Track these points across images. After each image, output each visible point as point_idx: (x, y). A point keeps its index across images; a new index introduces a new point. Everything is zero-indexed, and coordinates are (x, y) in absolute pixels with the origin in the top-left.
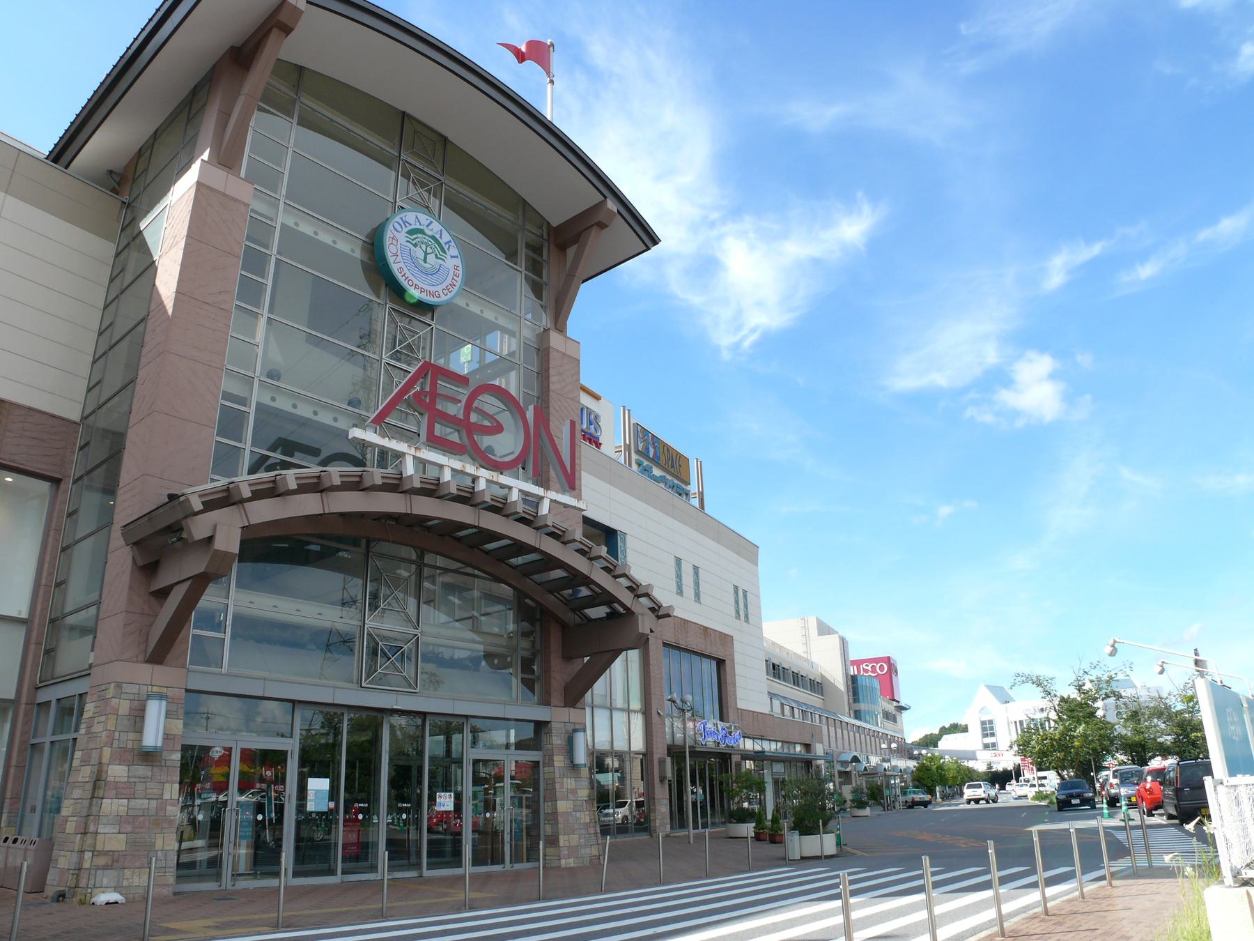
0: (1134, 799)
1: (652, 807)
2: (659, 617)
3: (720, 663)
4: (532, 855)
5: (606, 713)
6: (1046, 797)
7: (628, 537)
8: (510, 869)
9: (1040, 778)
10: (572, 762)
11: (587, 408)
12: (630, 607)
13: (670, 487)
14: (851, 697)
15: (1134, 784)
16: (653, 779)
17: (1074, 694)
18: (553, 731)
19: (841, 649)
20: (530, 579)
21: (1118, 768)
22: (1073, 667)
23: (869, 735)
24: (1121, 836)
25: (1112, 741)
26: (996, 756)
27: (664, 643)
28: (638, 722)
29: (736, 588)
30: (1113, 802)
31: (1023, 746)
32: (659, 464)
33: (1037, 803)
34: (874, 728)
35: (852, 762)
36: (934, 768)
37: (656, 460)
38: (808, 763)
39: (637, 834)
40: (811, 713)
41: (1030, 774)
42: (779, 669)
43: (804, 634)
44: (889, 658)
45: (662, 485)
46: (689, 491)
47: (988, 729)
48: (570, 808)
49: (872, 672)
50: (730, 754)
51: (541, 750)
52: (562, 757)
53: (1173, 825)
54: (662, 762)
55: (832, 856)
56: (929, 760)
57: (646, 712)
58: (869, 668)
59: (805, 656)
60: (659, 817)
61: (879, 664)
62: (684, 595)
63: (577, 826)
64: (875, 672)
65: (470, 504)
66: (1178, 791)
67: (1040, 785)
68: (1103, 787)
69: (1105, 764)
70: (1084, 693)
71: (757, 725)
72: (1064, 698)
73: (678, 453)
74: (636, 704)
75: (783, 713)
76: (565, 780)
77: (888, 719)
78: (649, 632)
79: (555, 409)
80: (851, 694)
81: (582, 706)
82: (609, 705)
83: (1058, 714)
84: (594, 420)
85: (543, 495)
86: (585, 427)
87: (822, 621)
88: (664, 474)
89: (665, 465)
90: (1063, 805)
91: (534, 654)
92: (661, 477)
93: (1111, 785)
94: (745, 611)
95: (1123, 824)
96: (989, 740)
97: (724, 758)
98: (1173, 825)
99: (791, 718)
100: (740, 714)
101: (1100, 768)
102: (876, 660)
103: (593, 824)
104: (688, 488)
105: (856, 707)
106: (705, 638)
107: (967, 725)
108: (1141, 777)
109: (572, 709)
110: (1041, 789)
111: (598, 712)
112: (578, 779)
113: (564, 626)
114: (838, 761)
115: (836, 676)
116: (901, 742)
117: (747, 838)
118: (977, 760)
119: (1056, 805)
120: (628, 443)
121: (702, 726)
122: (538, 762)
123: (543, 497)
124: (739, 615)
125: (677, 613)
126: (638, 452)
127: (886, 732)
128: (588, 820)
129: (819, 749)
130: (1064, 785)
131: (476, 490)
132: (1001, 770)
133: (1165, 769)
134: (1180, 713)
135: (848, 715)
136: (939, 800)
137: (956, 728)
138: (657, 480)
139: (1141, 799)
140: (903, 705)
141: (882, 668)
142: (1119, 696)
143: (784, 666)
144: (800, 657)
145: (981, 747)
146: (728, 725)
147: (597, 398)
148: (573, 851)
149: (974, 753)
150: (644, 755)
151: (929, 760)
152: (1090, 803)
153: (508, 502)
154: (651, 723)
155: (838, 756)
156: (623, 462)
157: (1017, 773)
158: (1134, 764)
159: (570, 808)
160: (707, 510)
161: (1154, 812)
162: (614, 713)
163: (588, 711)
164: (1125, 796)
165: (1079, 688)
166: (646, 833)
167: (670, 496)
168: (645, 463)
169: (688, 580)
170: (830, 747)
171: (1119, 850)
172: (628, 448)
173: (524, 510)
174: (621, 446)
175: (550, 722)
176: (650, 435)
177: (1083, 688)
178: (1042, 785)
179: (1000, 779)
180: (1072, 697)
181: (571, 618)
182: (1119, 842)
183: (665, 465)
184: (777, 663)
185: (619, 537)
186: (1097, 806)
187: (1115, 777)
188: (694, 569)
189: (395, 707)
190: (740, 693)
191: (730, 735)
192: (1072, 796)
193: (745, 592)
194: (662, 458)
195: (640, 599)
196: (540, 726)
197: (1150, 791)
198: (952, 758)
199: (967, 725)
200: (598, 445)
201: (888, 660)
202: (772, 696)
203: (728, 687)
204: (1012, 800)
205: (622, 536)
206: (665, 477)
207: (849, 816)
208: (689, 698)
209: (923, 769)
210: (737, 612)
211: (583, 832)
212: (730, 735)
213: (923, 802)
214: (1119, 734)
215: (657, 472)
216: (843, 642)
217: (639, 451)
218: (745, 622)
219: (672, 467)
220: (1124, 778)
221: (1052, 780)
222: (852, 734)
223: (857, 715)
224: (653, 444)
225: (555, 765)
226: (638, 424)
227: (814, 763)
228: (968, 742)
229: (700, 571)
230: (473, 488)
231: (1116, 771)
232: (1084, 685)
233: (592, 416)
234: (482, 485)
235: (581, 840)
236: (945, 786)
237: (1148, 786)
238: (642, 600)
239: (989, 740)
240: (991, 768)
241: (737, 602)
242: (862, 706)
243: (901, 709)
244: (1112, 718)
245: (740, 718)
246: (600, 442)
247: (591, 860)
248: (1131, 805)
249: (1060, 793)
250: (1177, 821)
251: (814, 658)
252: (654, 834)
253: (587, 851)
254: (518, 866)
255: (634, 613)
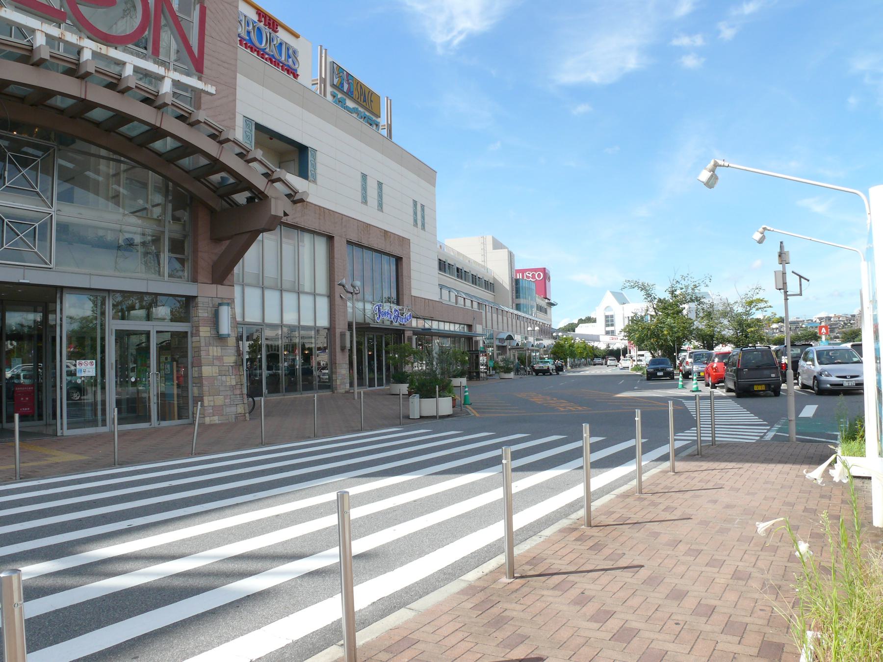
0: (702, 374)
1: (333, 370)
2: (295, 202)
3: (399, 260)
4: (183, 412)
5: (258, 292)
6: (641, 369)
7: (318, 153)
8: (158, 426)
9: (639, 355)
10: (218, 332)
11: (286, 43)
12: (263, 190)
13: (362, 118)
14: (514, 294)
15: (704, 363)
16: (335, 349)
17: (667, 296)
18: (199, 305)
19: (508, 260)
20: (175, 165)
21: (693, 350)
22: (669, 277)
23: (533, 323)
24: (690, 405)
25: (691, 332)
26: (613, 339)
27: (347, 241)
28: (323, 304)
29: (415, 203)
30: (687, 375)
31: (629, 332)
32: (353, 98)
33: (635, 373)
34: (530, 317)
35: (507, 339)
36: (567, 346)
37: (349, 94)
38: (469, 339)
39: (320, 391)
40: (492, 307)
41: (634, 352)
42: (462, 272)
43: (483, 248)
44: (545, 269)
45: (355, 115)
46: (379, 123)
47: (609, 321)
48: (216, 373)
49: (532, 278)
50: (404, 330)
51: (190, 322)
52: (209, 328)
53: (731, 397)
54: (343, 335)
55: (448, 416)
56: (564, 340)
57: (331, 296)
58: (530, 275)
59: (483, 264)
60: (340, 378)
61: (537, 273)
62: (369, 203)
63: (222, 388)
64: (535, 278)
65: (75, 76)
66: (738, 372)
67: (638, 361)
68: (681, 364)
69: (684, 347)
70: (675, 296)
71: (429, 310)
72: (660, 299)
73: (370, 91)
74: (322, 286)
75: (456, 303)
76: (211, 348)
77: (541, 311)
78: (282, 215)
79: (211, 11)
80: (514, 292)
81: (230, 284)
82: (297, 289)
83: (655, 311)
84: (293, 54)
85: (164, 74)
86: (284, 59)
87: (497, 240)
88: (356, 106)
89: (358, 99)
90: (652, 376)
91: (185, 236)
92: (353, 108)
93: (687, 363)
94: (422, 221)
95: (693, 394)
96: (610, 329)
97: (398, 334)
98: (731, 397)
99: (478, 310)
100: (413, 300)
101: (680, 351)
102: (536, 270)
103: (239, 386)
104: (378, 120)
105: (518, 301)
106: (385, 239)
107: (596, 318)
108: (710, 357)
109: (220, 287)
110: (639, 363)
111: (249, 291)
112: (224, 348)
113: (212, 211)
114: (496, 339)
115: (504, 279)
116: (547, 327)
117: (399, 395)
118: (600, 341)
119: (646, 375)
120: (323, 76)
121: (377, 307)
122: (187, 332)
123: (164, 77)
124: (417, 224)
125: (310, 199)
126: (333, 85)
127: (537, 319)
128: (234, 383)
129: (479, 329)
130: (653, 362)
131: (81, 62)
132: (616, 349)
133: (730, 353)
134: (740, 315)
135: (511, 307)
136: (569, 368)
137: (589, 320)
138: (351, 111)
139: (708, 375)
140: (552, 302)
141: (539, 276)
142: (700, 303)
143: (450, 263)
144: (479, 264)
145: (604, 333)
146: (400, 307)
147: (297, 36)
148: (217, 410)
149: (598, 336)
150: (328, 329)
151: (564, 340)
152: (670, 376)
153: (160, 94)
154: (334, 305)
155: (498, 334)
156: (386, 136)
157: (625, 351)
158: (705, 349)
159: (216, 373)
160: (393, 140)
161: (716, 385)
162: (366, 303)
163: (237, 289)
164: (696, 372)
165: (672, 292)
166: (328, 390)
167: (365, 127)
168: (340, 95)
169: (372, 192)
170: (492, 328)
171: (686, 421)
172: (324, 81)
173: (173, 103)
174: (317, 80)
175: (197, 297)
176: (345, 73)
177: (675, 293)
178: (641, 361)
179: (617, 354)
180: (667, 299)
181: (217, 204)
182: (686, 411)
183: (358, 99)
184: (460, 267)
185: (309, 153)
186: (675, 377)
187: (690, 357)
188: (378, 184)
189: (21, 281)
190: (414, 284)
191: (402, 316)
192: (658, 370)
193: (423, 206)
194: (356, 93)
195: (274, 184)
196: (189, 301)
197: (716, 370)
198: (581, 340)
199: (596, 318)
200: (296, 76)
201: (544, 270)
202: (441, 287)
203: (404, 279)
204: (619, 370)
205: (312, 152)
206: (357, 109)
207: (498, 378)
208: (358, 283)
209: (558, 346)
210: (415, 221)
211: (229, 393)
212: (402, 316)
213: (541, 370)
214: (697, 327)
215: (350, 104)
216: (511, 255)
217: (334, 84)
218: (422, 229)
219: (365, 101)
220: (697, 358)
221: (648, 356)
222: (510, 320)
223: (518, 307)
224: (348, 80)
225: (200, 335)
226: (334, 62)
227: (474, 339)
228: (597, 329)
229: (384, 187)
230: (79, 60)
231: (692, 353)
232: (676, 291)
233: (291, 51)
234: (86, 55)
235: (227, 401)
236: (574, 358)
237: (715, 365)
238: (278, 185)
239: (610, 329)
240: (609, 347)
241: (415, 213)
242: (522, 301)
243: (551, 304)
244: (693, 316)
245: (413, 303)
246: (298, 73)
247: (236, 418)
248: (700, 378)
249: (650, 367)
250: (734, 394)
251: (490, 266)
252: (336, 391)
253: (233, 409)
254: (164, 424)
255: (268, 197)
